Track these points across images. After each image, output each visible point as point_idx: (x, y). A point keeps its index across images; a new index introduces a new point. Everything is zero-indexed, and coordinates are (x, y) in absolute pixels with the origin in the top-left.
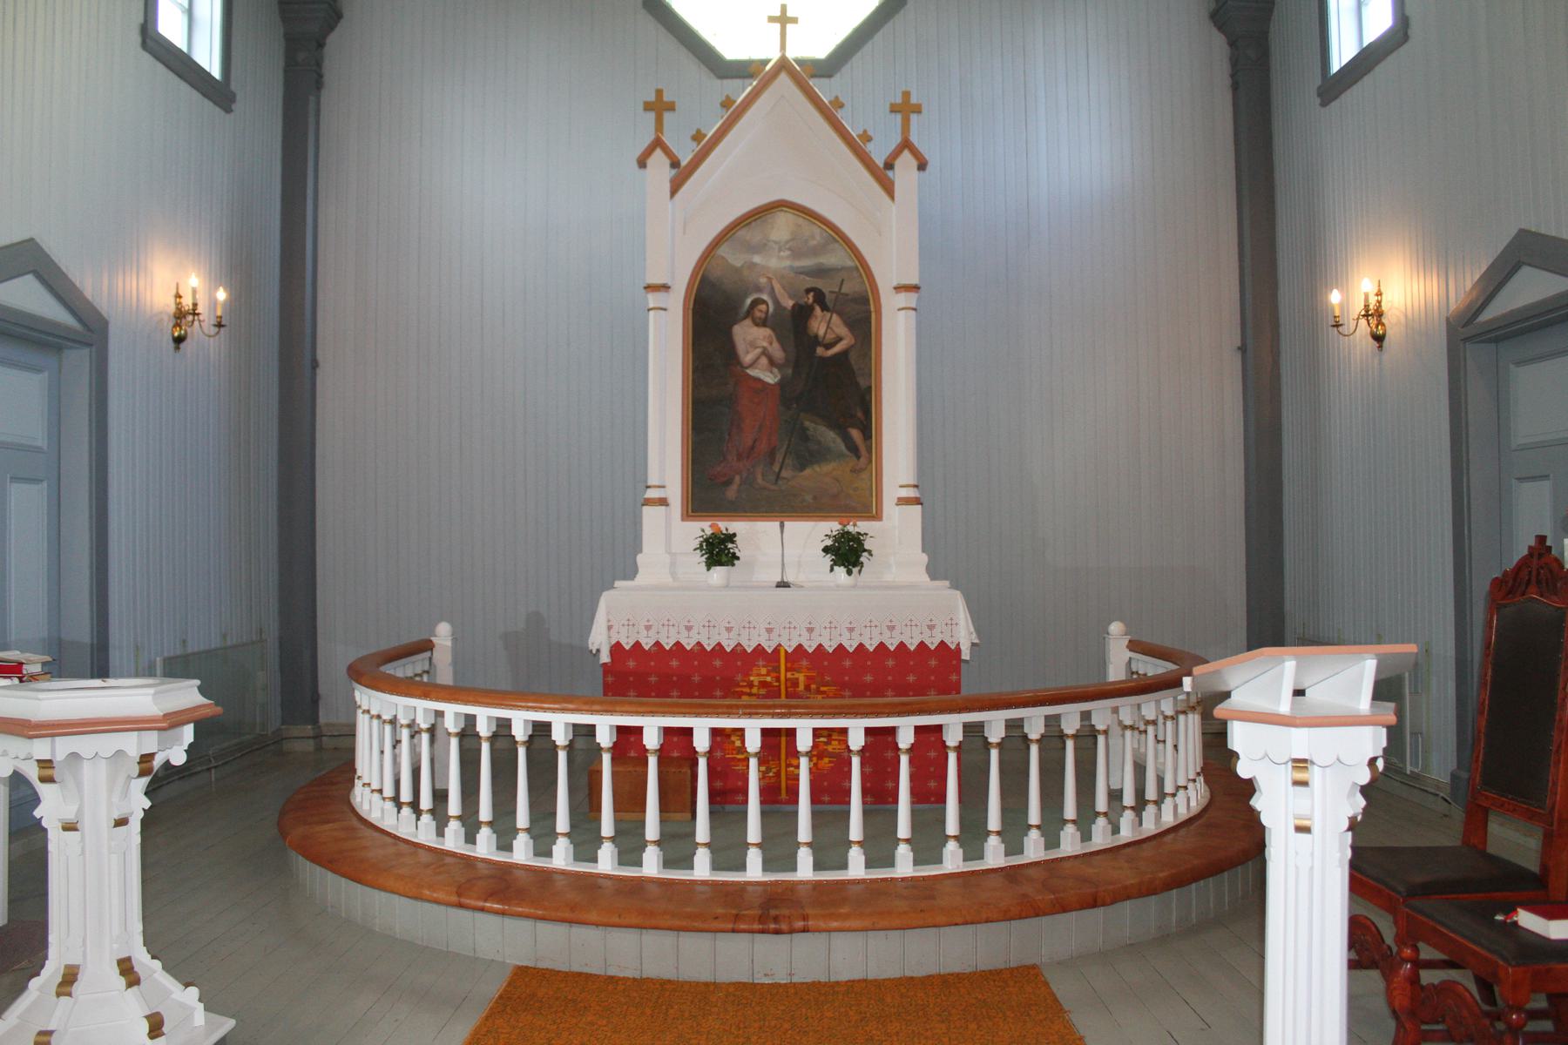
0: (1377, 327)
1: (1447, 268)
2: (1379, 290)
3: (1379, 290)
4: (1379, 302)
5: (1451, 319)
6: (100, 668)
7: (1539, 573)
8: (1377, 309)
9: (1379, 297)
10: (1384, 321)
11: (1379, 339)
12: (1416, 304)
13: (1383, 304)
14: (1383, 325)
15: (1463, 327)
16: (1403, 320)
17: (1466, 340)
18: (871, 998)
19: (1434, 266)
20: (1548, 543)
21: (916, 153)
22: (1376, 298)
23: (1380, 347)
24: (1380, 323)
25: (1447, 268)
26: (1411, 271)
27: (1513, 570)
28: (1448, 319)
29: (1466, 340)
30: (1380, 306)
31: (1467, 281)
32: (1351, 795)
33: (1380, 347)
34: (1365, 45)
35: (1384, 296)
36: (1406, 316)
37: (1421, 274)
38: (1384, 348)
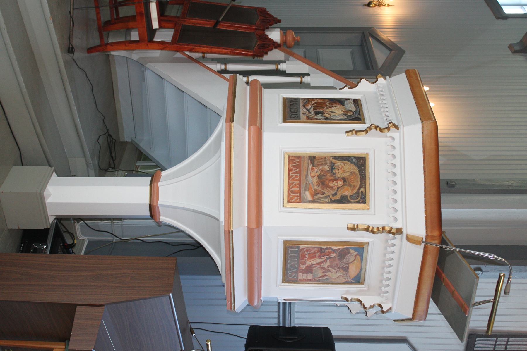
0: (374, 4)
1: (397, 28)
2: (390, 6)
3: (390, 6)
4: (385, 5)
5: (372, 29)
6: (224, 285)
7: (267, 44)
8: (381, 4)
9: (387, 5)
10: (376, 7)
11: (369, 5)
12: (382, 18)
13: (384, 7)
14: (374, 6)
15: (369, 33)
16: (375, 13)
17: (363, 33)
18: (348, 277)
19: (394, 24)
20: (278, 23)
21: (74, 253)
22: (387, 4)
23: (365, 5)
24: (376, 5)
25: (397, 28)
26: (395, 17)
27: (269, 13)
28: (373, 27)
29: (363, 33)
30: (383, 6)
31: (388, 36)
32: (348, 135)
33: (365, 5)
34: (502, 7)
35: (387, 7)
36: (377, 15)
37: (399, 20)
38: (364, 7)
